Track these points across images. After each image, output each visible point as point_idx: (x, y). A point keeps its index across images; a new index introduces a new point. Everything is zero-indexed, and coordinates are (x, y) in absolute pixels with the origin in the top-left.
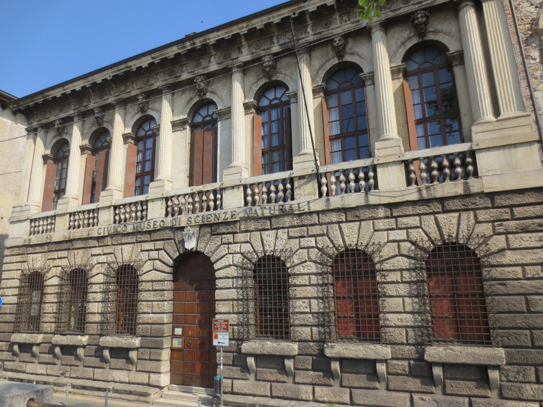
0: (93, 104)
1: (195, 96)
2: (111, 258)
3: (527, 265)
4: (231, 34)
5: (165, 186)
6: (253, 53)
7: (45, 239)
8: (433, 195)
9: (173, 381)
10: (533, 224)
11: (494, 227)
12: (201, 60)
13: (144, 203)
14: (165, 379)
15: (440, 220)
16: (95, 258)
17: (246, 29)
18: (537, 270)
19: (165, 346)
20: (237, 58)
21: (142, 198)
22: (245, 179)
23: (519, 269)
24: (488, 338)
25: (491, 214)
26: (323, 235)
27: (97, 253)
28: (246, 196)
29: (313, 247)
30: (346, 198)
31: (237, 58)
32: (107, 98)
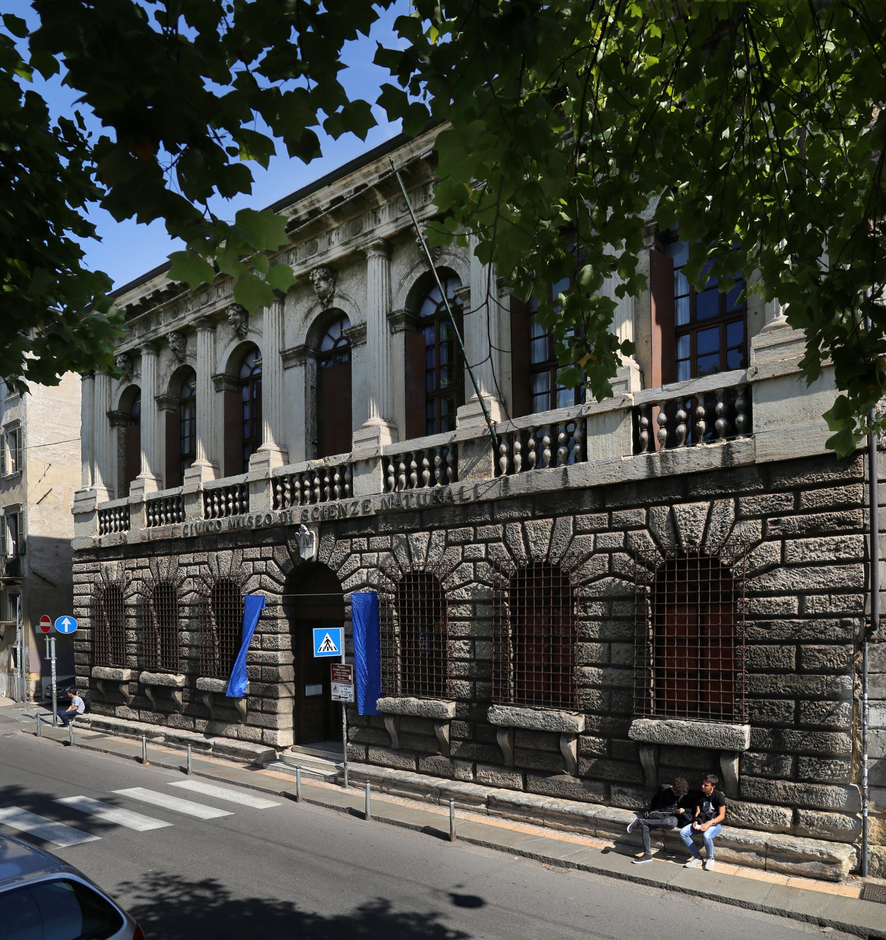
0: (165, 328)
1: (316, 305)
2: (204, 569)
3: (811, 592)
4: (352, 188)
5: (271, 461)
6: (397, 220)
7: (119, 540)
8: (671, 470)
10: (830, 520)
11: (764, 525)
12: (318, 240)
13: (244, 488)
14: (285, 737)
15: (678, 515)
16: (185, 569)
17: (376, 175)
18: (823, 600)
19: (281, 695)
20: (373, 231)
21: (239, 479)
22: (386, 447)
23: (794, 600)
24: (728, 709)
25: (764, 503)
26: (497, 540)
27: (186, 561)
28: (387, 474)
29: (481, 560)
30: (534, 477)
31: (373, 231)
32: (182, 315)
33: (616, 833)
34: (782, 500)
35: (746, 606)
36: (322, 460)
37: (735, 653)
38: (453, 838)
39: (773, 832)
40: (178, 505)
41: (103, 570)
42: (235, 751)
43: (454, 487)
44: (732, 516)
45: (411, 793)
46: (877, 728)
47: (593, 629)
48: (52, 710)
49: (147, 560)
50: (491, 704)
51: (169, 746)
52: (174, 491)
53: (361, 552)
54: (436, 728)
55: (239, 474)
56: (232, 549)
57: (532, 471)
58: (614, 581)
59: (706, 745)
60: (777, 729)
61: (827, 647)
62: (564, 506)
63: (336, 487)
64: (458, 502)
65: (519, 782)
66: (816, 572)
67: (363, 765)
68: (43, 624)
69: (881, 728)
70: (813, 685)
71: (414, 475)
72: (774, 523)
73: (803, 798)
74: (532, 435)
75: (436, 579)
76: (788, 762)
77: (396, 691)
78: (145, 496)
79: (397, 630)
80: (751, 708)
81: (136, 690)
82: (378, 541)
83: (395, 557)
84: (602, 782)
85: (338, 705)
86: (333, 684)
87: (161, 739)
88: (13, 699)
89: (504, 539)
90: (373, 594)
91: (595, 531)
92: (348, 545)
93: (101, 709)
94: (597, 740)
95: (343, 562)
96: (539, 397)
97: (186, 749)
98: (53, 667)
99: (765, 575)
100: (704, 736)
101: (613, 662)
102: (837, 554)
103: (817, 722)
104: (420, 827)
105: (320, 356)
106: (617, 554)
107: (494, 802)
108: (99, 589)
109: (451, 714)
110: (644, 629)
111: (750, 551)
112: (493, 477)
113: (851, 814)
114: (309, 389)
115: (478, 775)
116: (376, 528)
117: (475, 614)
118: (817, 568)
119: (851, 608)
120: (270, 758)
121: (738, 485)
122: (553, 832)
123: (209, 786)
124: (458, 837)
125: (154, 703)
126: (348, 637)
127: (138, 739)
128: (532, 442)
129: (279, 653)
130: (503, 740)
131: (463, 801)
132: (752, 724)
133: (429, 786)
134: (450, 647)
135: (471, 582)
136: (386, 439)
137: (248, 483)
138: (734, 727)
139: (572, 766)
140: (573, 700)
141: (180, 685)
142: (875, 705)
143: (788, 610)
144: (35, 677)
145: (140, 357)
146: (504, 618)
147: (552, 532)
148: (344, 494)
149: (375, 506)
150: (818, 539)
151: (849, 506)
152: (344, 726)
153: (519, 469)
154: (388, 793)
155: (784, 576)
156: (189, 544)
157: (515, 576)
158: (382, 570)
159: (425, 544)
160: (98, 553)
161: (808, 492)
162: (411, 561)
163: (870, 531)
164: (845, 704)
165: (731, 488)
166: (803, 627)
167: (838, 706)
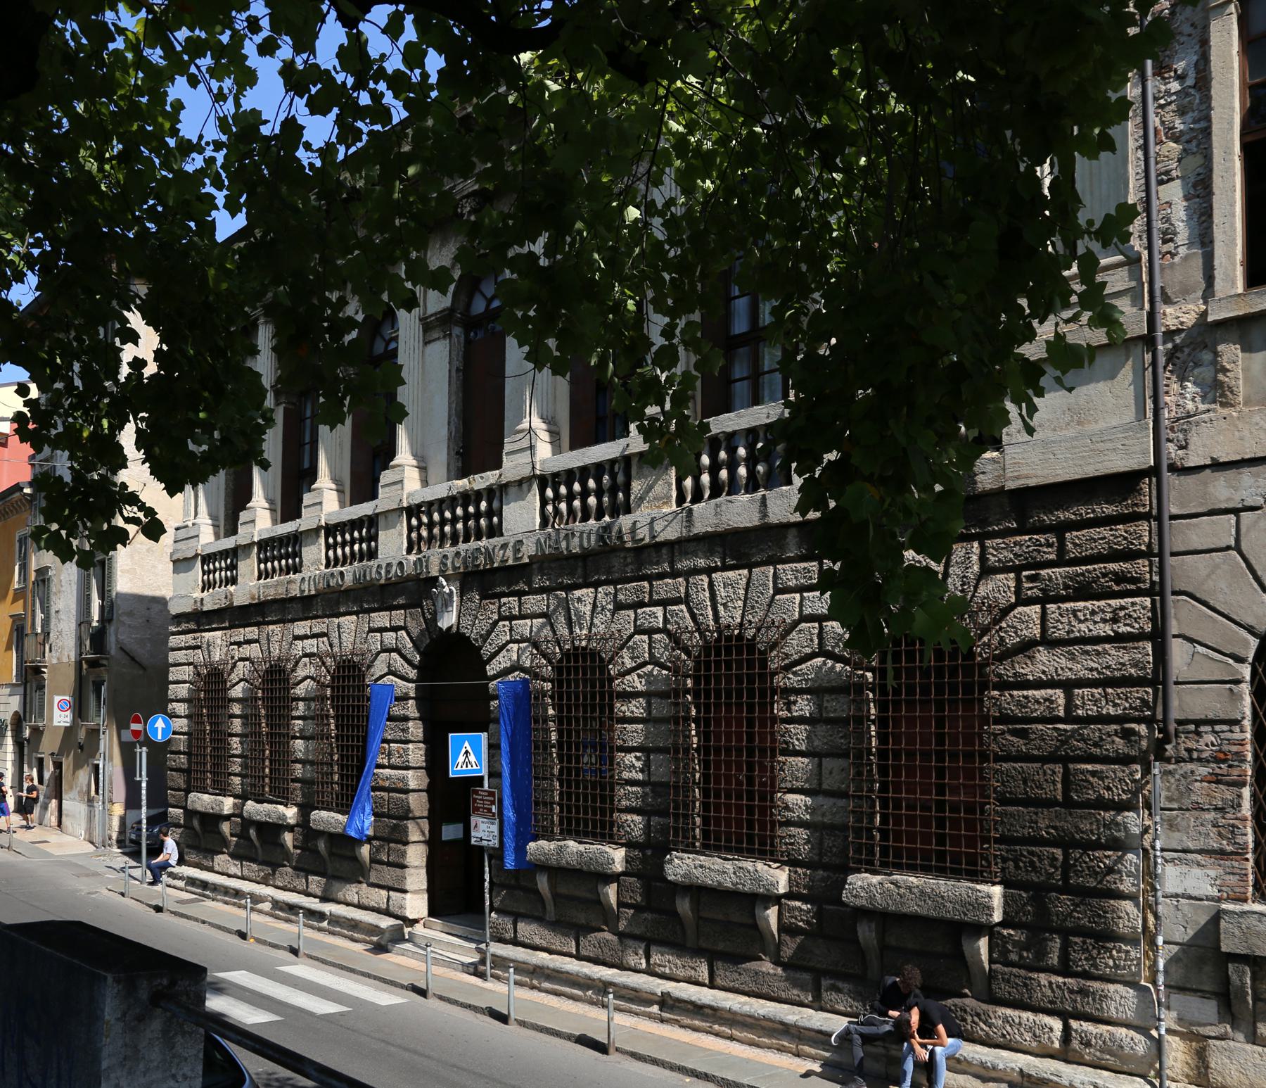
5: (405, 481)
9: (433, 912)
10: (1104, 575)
13: (372, 522)
14: (416, 904)
16: (299, 643)
21: (366, 509)
22: (543, 462)
23: (1059, 695)
24: (972, 860)
25: (1017, 549)
26: (677, 601)
29: (658, 631)
30: (724, 508)
33: (824, 1050)
34: (1041, 545)
35: (995, 704)
36: (466, 480)
37: (981, 774)
38: (611, 1050)
39: (1036, 1055)
40: (294, 547)
41: (205, 646)
42: (354, 925)
43: (625, 521)
44: (976, 568)
45: (562, 988)
46: (1177, 896)
47: (798, 736)
48: (139, 861)
49: (256, 629)
50: (669, 851)
51: (277, 917)
52: (290, 527)
53: (511, 618)
54: (600, 887)
55: (367, 501)
56: (357, 613)
57: (723, 498)
58: (824, 663)
59: (943, 914)
60: (1040, 891)
61: (1104, 768)
62: (762, 550)
63: (482, 521)
64: (629, 545)
65: (703, 972)
66: (1087, 653)
67: (510, 947)
68: (134, 726)
69: (1183, 896)
70: (1085, 826)
71: (577, 503)
72: (1031, 579)
73: (1075, 1001)
74: (723, 446)
75: (602, 660)
76: (1056, 944)
77: (552, 831)
78: (256, 534)
79: (554, 736)
80: (1004, 860)
81: (238, 830)
82: (534, 603)
83: (552, 626)
84: (811, 974)
85: (481, 849)
86: (474, 820)
87: (266, 906)
88: (92, 843)
89: (686, 600)
90: (525, 680)
91: (801, 589)
92: (494, 607)
93: (196, 860)
94: (804, 907)
95: (489, 633)
96: (738, 384)
97: (296, 922)
98: (144, 792)
99: (1020, 657)
100: (940, 900)
101: (825, 786)
102: (1115, 627)
103: (1092, 883)
104: (574, 1036)
105: (471, 324)
106: (829, 623)
107: (671, 1002)
108: (199, 674)
109: (619, 867)
110: (862, 736)
111: (1000, 620)
112: (674, 507)
113: (1143, 1031)
114: (454, 374)
115: (652, 961)
116: (529, 583)
117: (649, 713)
118: (1089, 648)
119: (1135, 709)
120: (398, 937)
121: (983, 522)
122: (743, 1047)
123: (324, 973)
124: (617, 1050)
125: (260, 851)
126: (493, 747)
127: (240, 906)
128: (723, 455)
129: (410, 773)
130: (684, 906)
131: (631, 1000)
132: (1006, 883)
133: (589, 978)
134: (618, 764)
135: (644, 664)
136: (544, 450)
137: (377, 515)
138: (978, 887)
139: (772, 948)
140: (772, 845)
141: (292, 822)
142: (1172, 860)
143: (1051, 710)
144: (118, 810)
145: (257, 326)
146: (687, 719)
147: (747, 590)
148: (495, 531)
149: (529, 549)
150: (1088, 604)
151: (1129, 555)
152: (487, 884)
153: (706, 496)
154: (540, 990)
155: (1044, 659)
156: (304, 607)
157: (700, 655)
158: (536, 645)
159: (589, 607)
160: (200, 619)
161: (1075, 533)
162: (571, 632)
163: (1157, 591)
164: (1130, 856)
165: (974, 526)
166: (1070, 737)
167: (1121, 858)
